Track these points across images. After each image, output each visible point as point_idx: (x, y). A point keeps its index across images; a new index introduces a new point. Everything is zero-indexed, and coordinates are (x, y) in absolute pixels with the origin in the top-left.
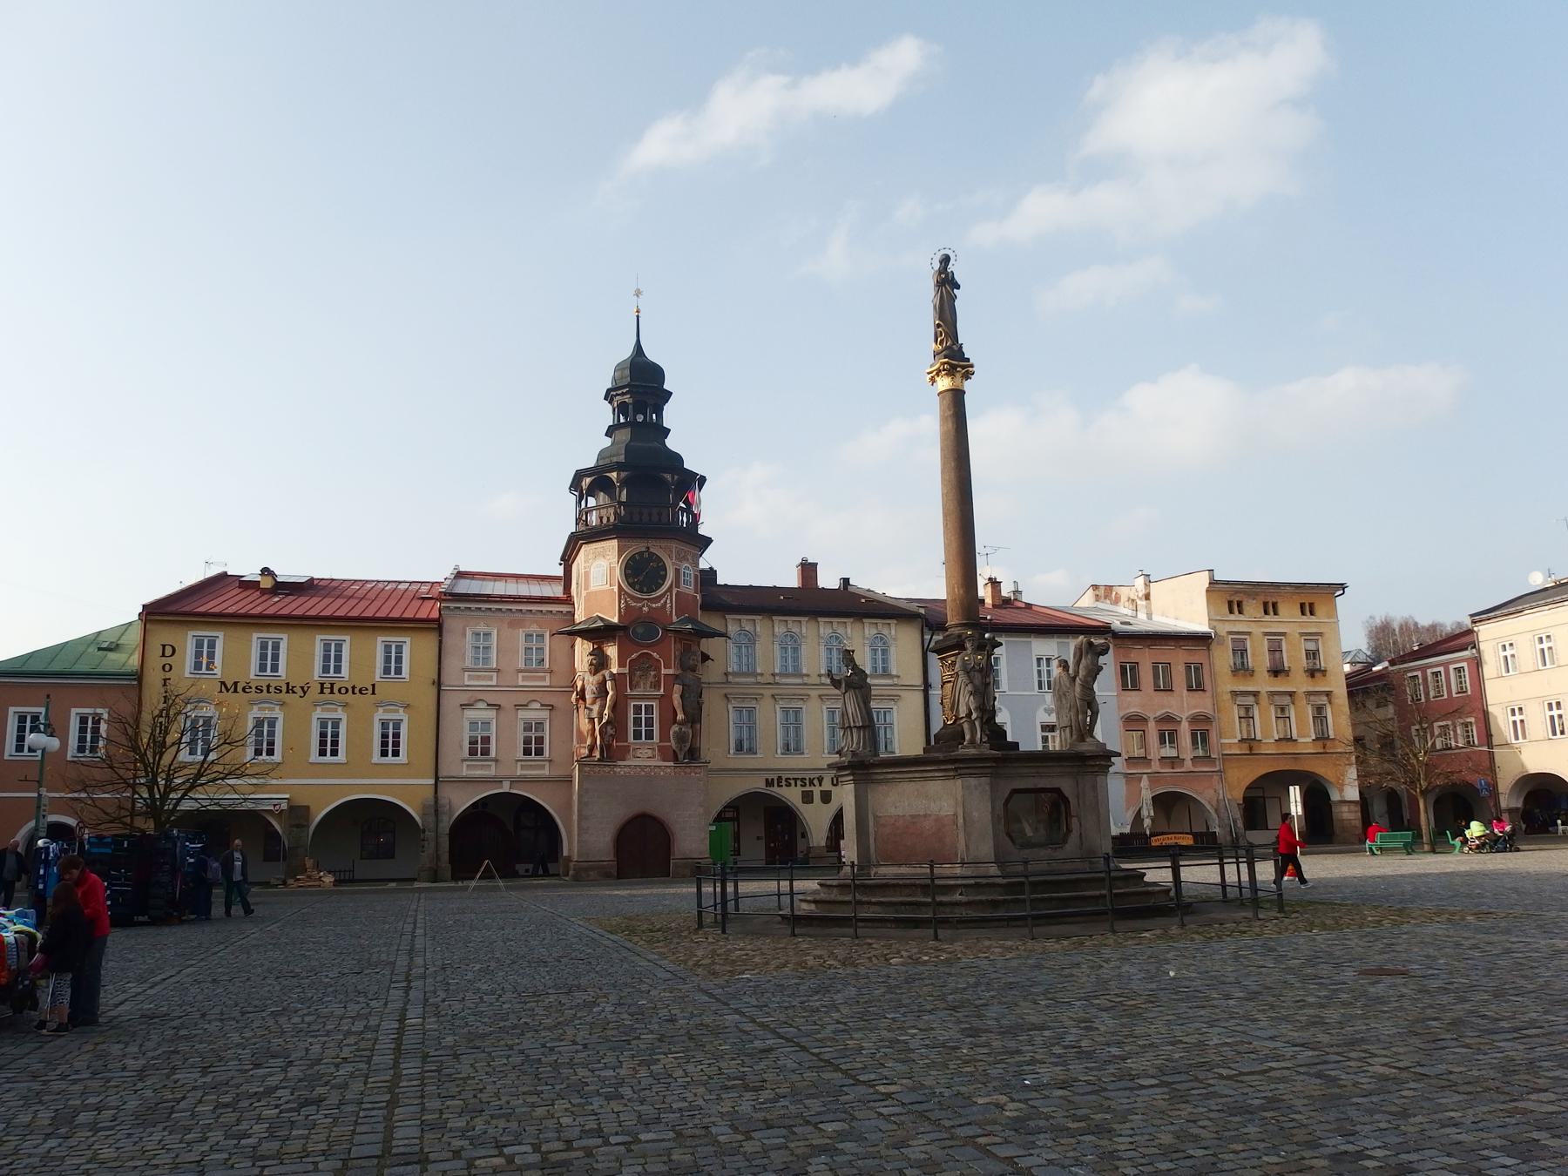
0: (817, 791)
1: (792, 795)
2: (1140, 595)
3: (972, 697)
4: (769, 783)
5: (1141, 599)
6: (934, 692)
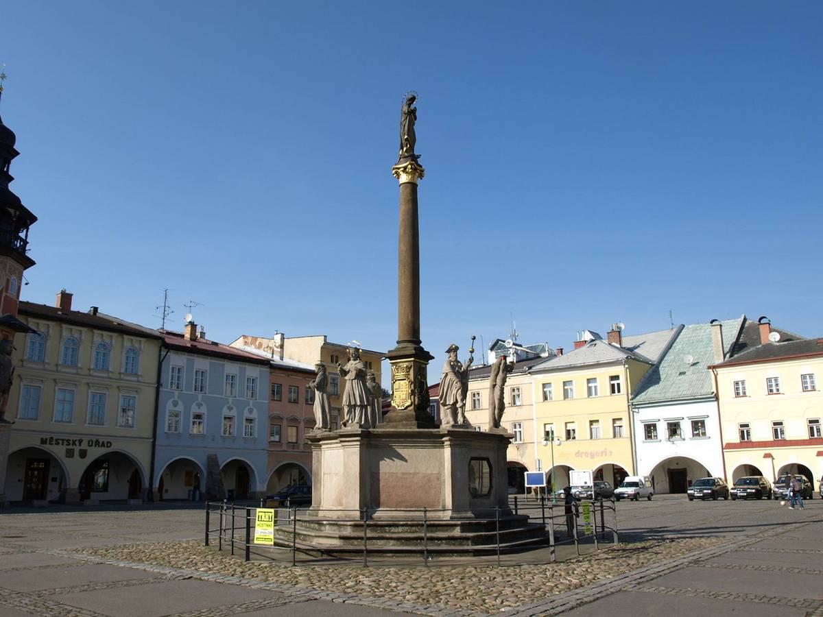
0: (77, 449)
1: (59, 451)
2: (277, 345)
4: (43, 441)
5: (277, 347)
6: (163, 389)
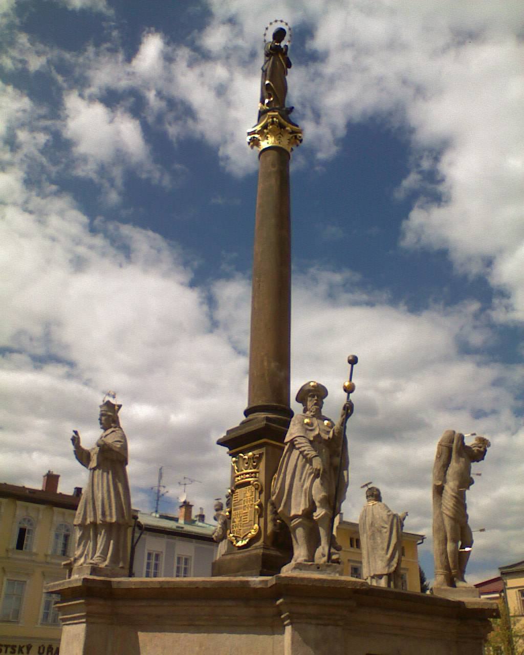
3: (318, 481)
